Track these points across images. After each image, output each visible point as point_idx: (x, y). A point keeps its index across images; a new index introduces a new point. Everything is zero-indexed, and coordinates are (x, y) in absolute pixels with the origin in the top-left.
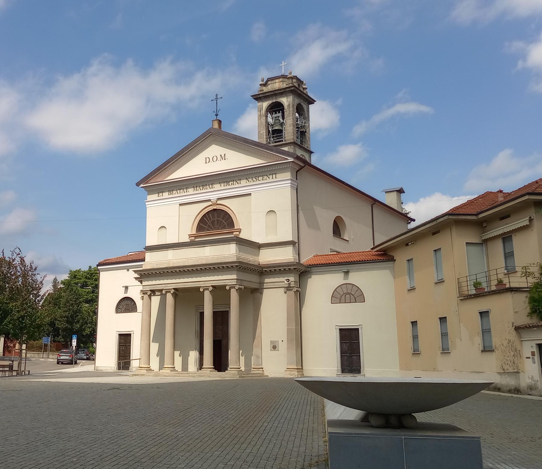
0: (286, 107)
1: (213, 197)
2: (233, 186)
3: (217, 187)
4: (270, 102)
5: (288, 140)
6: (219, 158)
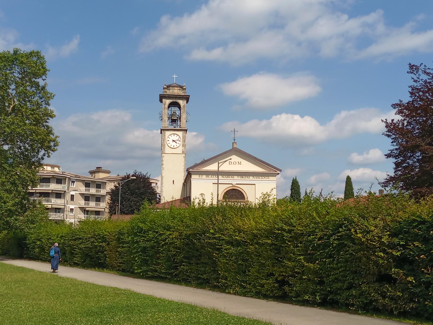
0: (182, 107)
1: (234, 183)
2: (245, 179)
3: (236, 177)
4: (171, 101)
5: (183, 126)
6: (237, 163)
